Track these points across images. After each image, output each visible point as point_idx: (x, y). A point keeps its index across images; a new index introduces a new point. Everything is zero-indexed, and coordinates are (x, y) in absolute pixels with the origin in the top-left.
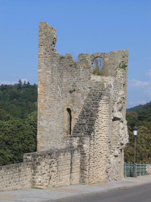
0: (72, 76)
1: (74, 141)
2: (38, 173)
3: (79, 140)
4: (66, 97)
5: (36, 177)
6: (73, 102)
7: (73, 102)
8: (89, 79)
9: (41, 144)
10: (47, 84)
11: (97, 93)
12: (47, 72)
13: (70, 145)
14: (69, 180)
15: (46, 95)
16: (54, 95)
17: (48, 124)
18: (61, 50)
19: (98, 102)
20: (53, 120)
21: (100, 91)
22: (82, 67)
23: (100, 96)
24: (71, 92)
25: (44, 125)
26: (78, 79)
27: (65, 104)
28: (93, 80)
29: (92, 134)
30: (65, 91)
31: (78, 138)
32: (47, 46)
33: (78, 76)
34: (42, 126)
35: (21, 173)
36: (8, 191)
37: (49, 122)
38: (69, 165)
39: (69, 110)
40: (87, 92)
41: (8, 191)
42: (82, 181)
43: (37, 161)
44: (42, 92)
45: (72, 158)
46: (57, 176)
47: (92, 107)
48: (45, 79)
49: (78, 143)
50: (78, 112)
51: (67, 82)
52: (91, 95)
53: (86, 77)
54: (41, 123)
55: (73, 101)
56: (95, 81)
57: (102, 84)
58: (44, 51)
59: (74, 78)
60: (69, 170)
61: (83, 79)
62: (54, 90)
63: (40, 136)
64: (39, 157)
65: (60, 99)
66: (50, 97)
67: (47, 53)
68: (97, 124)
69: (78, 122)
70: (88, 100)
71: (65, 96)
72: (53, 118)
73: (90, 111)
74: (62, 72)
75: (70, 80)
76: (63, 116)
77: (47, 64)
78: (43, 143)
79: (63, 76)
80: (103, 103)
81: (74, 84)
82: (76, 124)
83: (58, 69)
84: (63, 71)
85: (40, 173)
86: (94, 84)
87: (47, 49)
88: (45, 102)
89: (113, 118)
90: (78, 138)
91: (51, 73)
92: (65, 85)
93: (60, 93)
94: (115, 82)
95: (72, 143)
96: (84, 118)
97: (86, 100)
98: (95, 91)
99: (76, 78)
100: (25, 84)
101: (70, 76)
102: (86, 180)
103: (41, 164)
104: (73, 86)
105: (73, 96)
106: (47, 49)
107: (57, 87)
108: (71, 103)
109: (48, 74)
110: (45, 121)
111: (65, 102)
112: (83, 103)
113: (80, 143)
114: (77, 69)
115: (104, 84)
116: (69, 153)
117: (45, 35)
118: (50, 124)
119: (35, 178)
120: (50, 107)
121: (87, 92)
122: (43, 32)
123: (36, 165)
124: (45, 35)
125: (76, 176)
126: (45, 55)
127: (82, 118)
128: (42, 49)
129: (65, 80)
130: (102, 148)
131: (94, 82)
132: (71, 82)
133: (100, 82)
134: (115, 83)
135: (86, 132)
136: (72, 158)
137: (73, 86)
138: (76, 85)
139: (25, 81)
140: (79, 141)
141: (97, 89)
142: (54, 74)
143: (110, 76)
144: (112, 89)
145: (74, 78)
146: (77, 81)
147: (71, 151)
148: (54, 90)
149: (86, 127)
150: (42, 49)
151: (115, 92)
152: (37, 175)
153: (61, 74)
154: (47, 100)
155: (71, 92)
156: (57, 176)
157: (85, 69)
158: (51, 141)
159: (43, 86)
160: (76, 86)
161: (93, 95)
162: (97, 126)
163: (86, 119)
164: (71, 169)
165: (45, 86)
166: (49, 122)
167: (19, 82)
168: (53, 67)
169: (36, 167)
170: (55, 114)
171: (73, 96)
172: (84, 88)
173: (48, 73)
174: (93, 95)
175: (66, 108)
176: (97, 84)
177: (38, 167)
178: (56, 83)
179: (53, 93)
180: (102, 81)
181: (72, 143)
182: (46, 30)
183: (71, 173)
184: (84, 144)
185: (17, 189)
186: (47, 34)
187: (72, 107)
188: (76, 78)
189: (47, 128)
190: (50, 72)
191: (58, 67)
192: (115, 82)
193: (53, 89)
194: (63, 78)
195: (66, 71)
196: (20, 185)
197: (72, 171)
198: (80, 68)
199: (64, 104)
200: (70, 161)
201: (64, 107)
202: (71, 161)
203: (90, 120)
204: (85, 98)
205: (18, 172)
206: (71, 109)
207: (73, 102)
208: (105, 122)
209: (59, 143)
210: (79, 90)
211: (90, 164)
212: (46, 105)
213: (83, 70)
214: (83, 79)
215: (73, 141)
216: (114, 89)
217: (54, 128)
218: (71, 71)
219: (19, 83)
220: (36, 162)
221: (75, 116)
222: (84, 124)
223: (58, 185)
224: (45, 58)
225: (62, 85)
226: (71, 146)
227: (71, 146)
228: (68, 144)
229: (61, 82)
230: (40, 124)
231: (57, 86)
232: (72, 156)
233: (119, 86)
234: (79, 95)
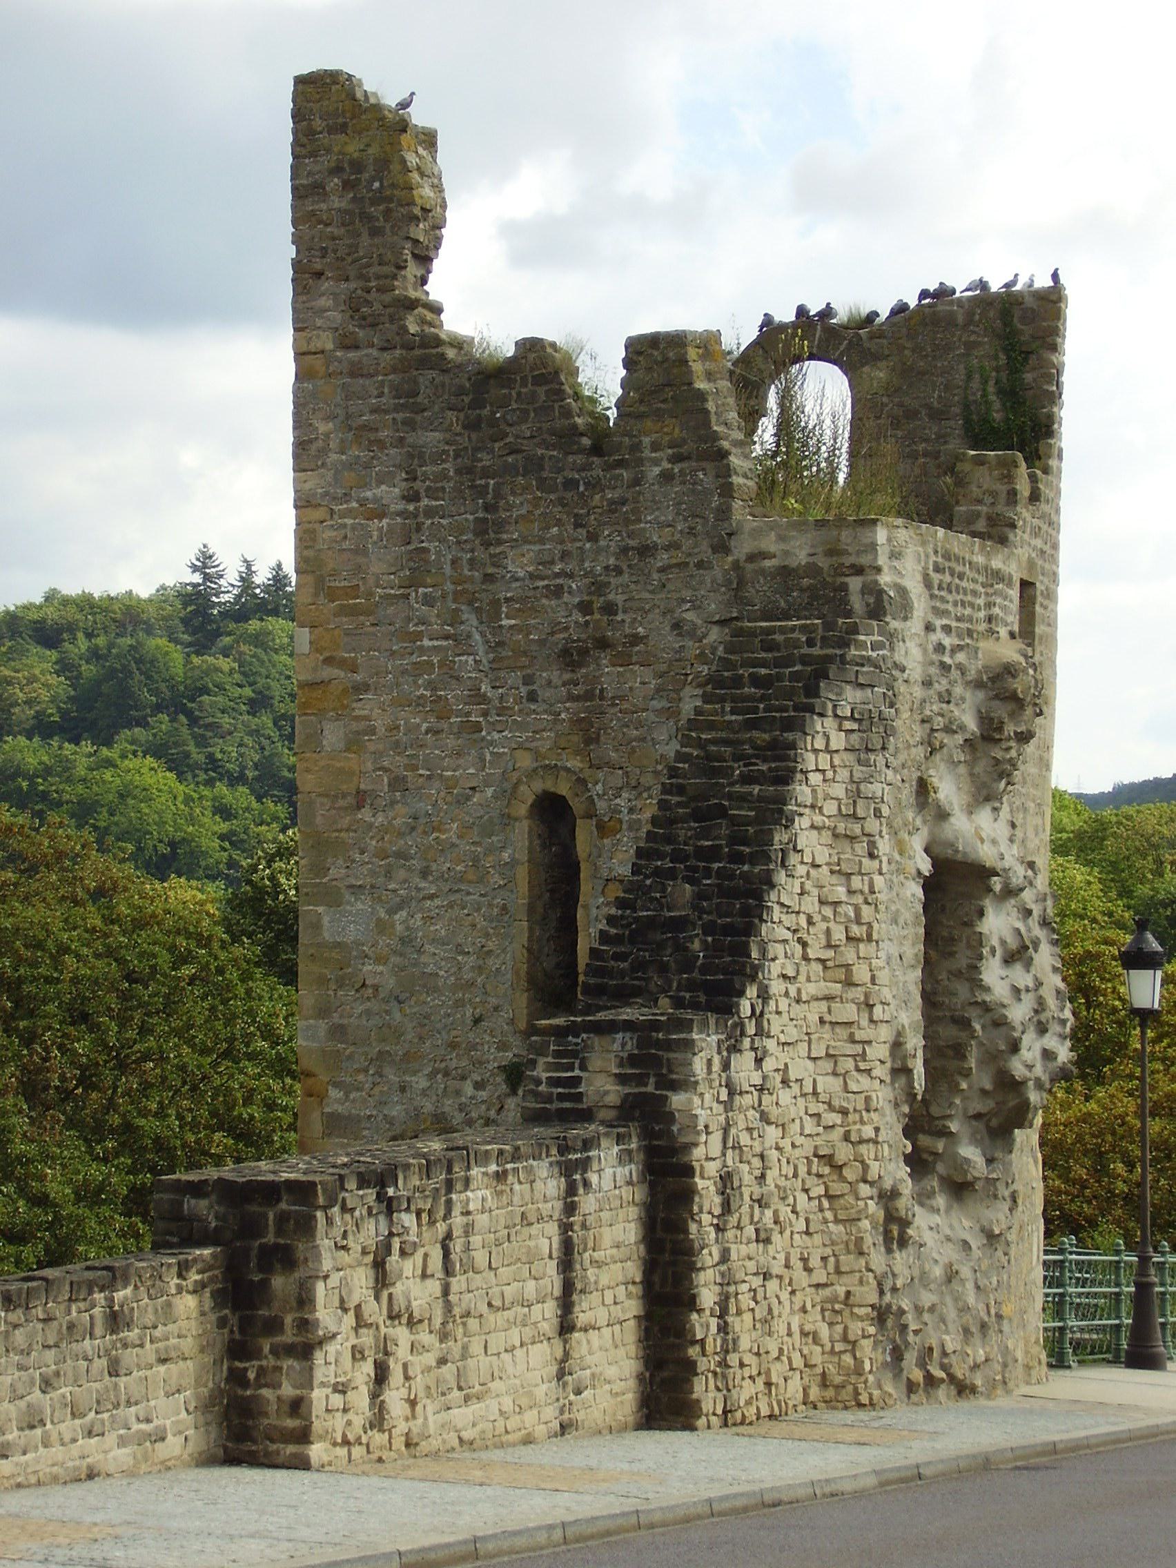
0: (577, 525)
1: (595, 1062)
2: (278, 1339)
3: (631, 1056)
4: (532, 697)
5: (261, 1371)
6: (588, 741)
7: (591, 740)
8: (722, 548)
9: (334, 1093)
10: (370, 594)
11: (786, 662)
12: (369, 494)
13: (561, 1097)
14: (544, 1390)
15: (365, 688)
16: (431, 685)
17: (382, 927)
18: (478, 294)
19: (789, 736)
20: (431, 897)
21: (810, 643)
22: (655, 447)
23: (812, 691)
24: (571, 657)
25: (352, 933)
26: (625, 550)
27: (525, 761)
28: (751, 558)
29: (745, 1008)
30: (525, 653)
31: (622, 1044)
32: (361, 277)
33: (627, 522)
34: (338, 945)
35: (133, 1335)
36: (19, 1486)
37: (392, 911)
38: (552, 1268)
39: (553, 813)
40: (702, 658)
41: (19, 1486)
42: (665, 1399)
43: (270, 1238)
44: (328, 661)
45: (570, 1209)
46: (442, 1361)
47: (747, 779)
48: (356, 552)
49: (622, 1079)
50: (634, 826)
51: (532, 576)
52: (737, 682)
53: (691, 532)
54: (326, 920)
55: (588, 734)
56: (768, 563)
57: (824, 584)
58: (336, 316)
59: (593, 537)
60: (550, 1309)
61: (674, 546)
62: (426, 643)
63: (322, 1026)
64: (283, 1206)
65: (485, 714)
66: (403, 702)
67: (361, 334)
68: (789, 920)
69: (621, 903)
70: (711, 726)
71: (524, 690)
72: (425, 874)
73: (722, 812)
74: (498, 495)
75: (565, 555)
76: (506, 856)
77: (365, 427)
78: (347, 1088)
79: (500, 526)
80: (838, 740)
81: (599, 587)
82: (611, 920)
83: (458, 472)
84: (506, 489)
85: (289, 1336)
86: (759, 592)
87: (368, 303)
88: (353, 744)
89: (926, 866)
90: (622, 1044)
91: (401, 506)
92: (525, 606)
93: (485, 665)
94: (937, 569)
95: (576, 1081)
96: (672, 874)
97: (692, 724)
98: (770, 647)
99: (610, 539)
100: (246, 580)
101: (559, 523)
102: (706, 1393)
103: (300, 1255)
104: (585, 608)
105: (588, 696)
106: (368, 303)
107: (455, 619)
108: (577, 752)
109: (381, 516)
110: (362, 905)
111: (520, 747)
112: (671, 749)
113: (641, 1080)
114: (621, 464)
115: (844, 588)
116: (542, 1168)
117: (347, 185)
118: (399, 928)
119: (251, 1375)
120: (398, 783)
121: (702, 658)
122: (326, 161)
123: (261, 1269)
124: (347, 185)
125: (611, 1355)
126: (351, 355)
127: (657, 872)
128: (324, 302)
129: (520, 563)
130: (836, 1118)
131: (762, 572)
132: (571, 576)
133: (812, 570)
134: (936, 577)
135: (691, 986)
136: (570, 1209)
137: (585, 608)
138: (611, 597)
139: (248, 565)
140: (633, 1060)
141: (782, 630)
142: (430, 512)
143: (900, 521)
144: (915, 626)
145: (593, 537)
146: (619, 571)
147: (563, 1150)
148: (426, 643)
149: (696, 945)
150: (324, 302)
151: (940, 648)
152: (267, 1349)
153: (487, 508)
154: (372, 731)
155: (571, 657)
156: (442, 1361)
157: (685, 465)
158: (415, 1073)
159: (344, 611)
160: (610, 609)
161: (756, 681)
162: (789, 935)
163: (691, 881)
164: (566, 1303)
165: (353, 611)
166: (400, 907)
167: (195, 569)
168: (417, 456)
169: (265, 1284)
170: (446, 848)
171: (588, 696)
172: (676, 626)
173: (376, 500)
174: (756, 681)
175: (528, 794)
176: (787, 591)
177: (278, 1282)
178: (449, 587)
179: (420, 669)
180: (823, 562)
181: (576, 1081)
182: (353, 148)
183: (566, 1327)
184: (675, 1086)
185: (91, 1476)
186: (366, 175)
187: (582, 782)
188: (610, 539)
189: (379, 960)
190: (389, 493)
191: (457, 456)
192: (937, 569)
193: (419, 636)
194: (500, 542)
195: (525, 489)
196: (122, 1442)
197: (581, 1317)
198: (640, 462)
199: (522, 748)
200: (553, 1229)
201: (516, 786)
202: (566, 1228)
203: (724, 893)
204: (690, 703)
205: (99, 1331)
206: (577, 805)
207: (588, 741)
208: (859, 899)
209: (479, 1086)
210: (636, 639)
211: (734, 1256)
212: (369, 766)
213: (666, 477)
214: (674, 546)
215: (583, 1068)
216: (929, 628)
217: (434, 960)
218: (570, 484)
219: (197, 578)
220: (263, 1247)
221: (609, 861)
222: (679, 924)
223: (453, 1435)
224: (352, 374)
225: (496, 604)
226: (567, 1105)
227: (567, 1105)
228: (542, 1088)
229: (489, 578)
230: (317, 926)
231: (457, 610)
232: (571, 1190)
233: (981, 601)
234: (641, 681)
